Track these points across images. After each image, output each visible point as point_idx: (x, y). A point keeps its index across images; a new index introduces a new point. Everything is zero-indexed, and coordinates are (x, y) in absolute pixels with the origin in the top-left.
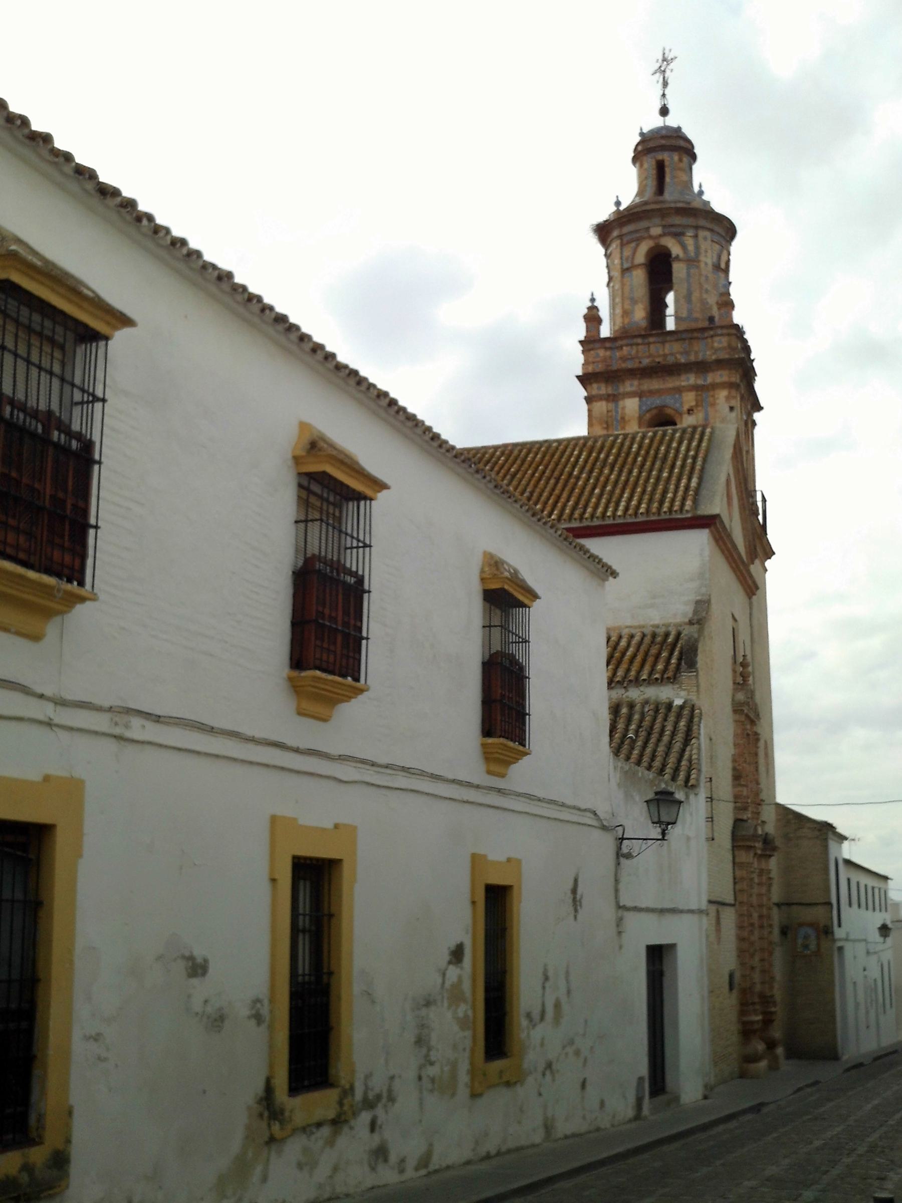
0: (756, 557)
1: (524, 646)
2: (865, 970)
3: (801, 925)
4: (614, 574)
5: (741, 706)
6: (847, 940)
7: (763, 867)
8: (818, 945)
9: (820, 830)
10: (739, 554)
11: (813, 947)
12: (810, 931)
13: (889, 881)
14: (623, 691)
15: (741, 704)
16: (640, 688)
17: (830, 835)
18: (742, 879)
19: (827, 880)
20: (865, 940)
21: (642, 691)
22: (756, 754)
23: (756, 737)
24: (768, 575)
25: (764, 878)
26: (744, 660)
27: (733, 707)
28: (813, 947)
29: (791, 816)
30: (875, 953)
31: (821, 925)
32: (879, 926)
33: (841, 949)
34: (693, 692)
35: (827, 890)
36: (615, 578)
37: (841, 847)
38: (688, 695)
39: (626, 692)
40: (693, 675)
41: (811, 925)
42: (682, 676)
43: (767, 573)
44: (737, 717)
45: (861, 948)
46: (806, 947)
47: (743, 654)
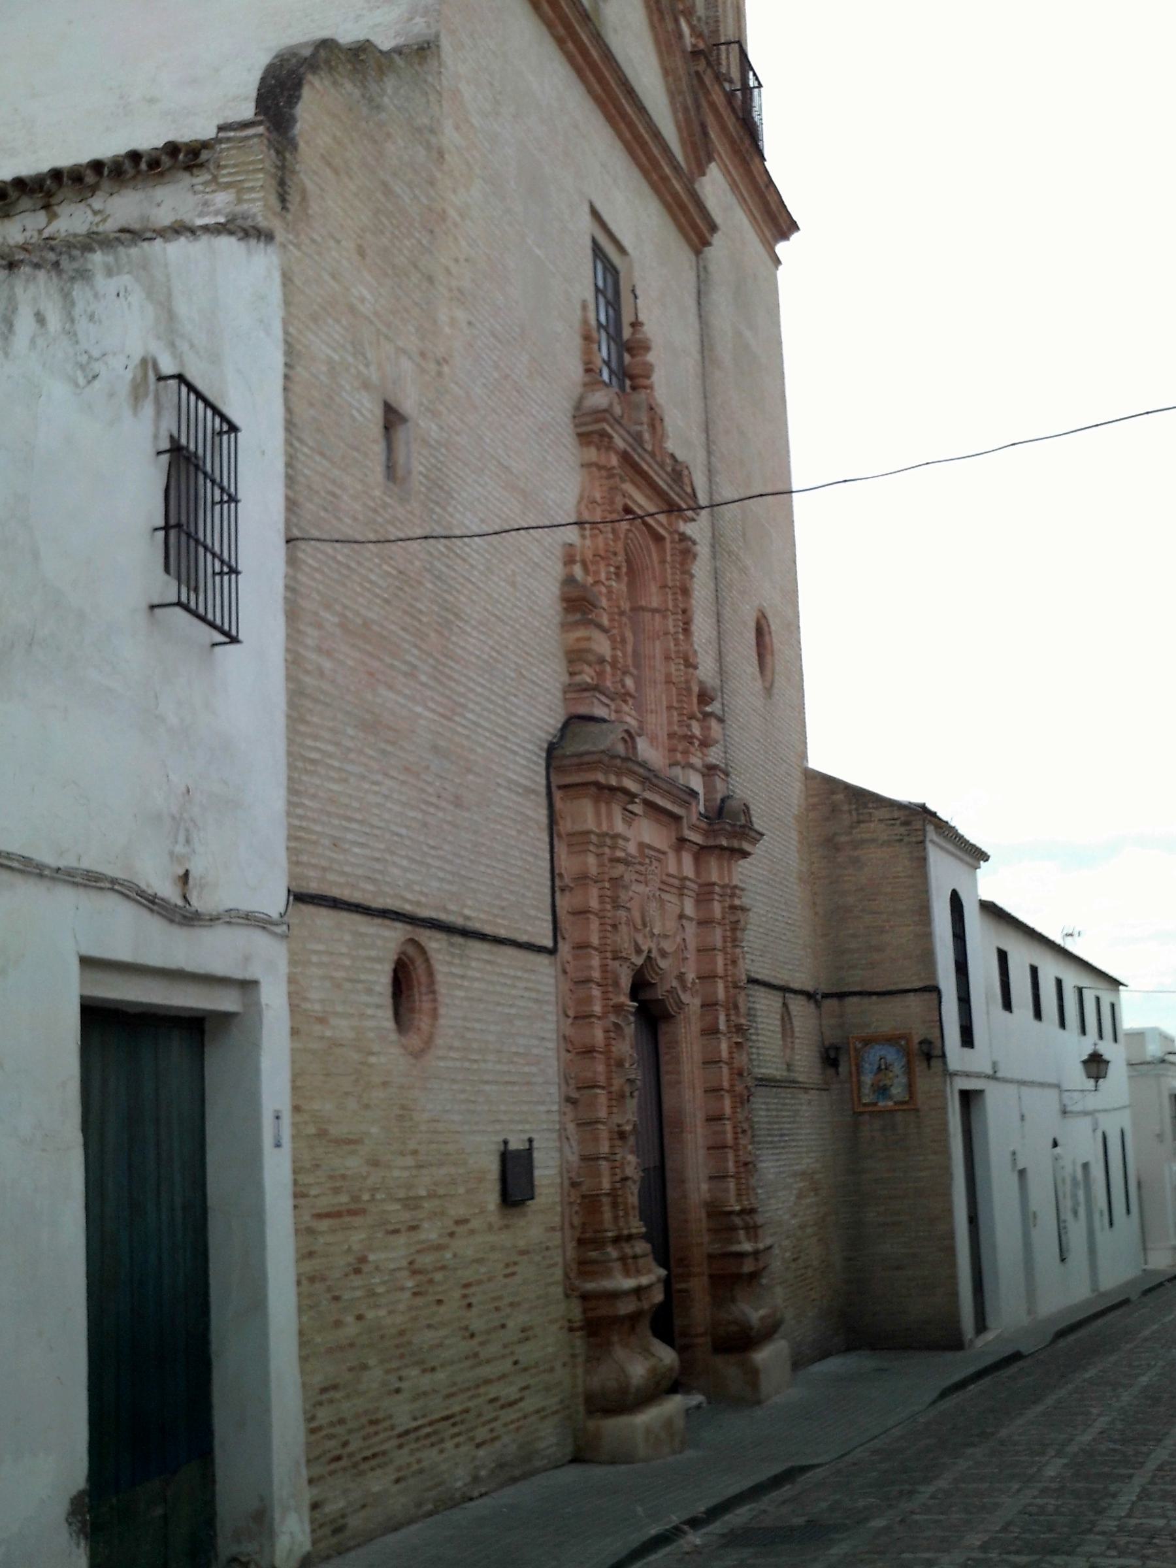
0: (710, 159)
1: (232, 439)
2: (1055, 1144)
3: (868, 1042)
4: (984, 857)
5: (597, 421)
6: (993, 1077)
7: (714, 878)
8: (910, 1087)
9: (906, 823)
10: (657, 135)
11: (898, 1091)
12: (890, 1054)
13: (1121, 988)
14: (41, 217)
15: (600, 415)
16: (90, 201)
17: (930, 830)
18: (583, 878)
19: (926, 936)
20: (1058, 1086)
21: (95, 213)
22: (685, 591)
23: (683, 545)
24: (782, 273)
25: (717, 909)
26: (633, 334)
27: (576, 426)
28: (898, 1091)
29: (840, 797)
30: (1086, 1113)
31: (916, 1040)
32: (1085, 1057)
33: (968, 1098)
34: (252, 189)
35: (928, 957)
36: (987, 860)
37: (975, 872)
38: (240, 201)
39: (49, 223)
40: (255, 136)
41: (891, 1040)
42: (222, 151)
43: (780, 268)
44: (592, 454)
45: (1043, 1104)
46: (882, 1090)
47: (633, 319)
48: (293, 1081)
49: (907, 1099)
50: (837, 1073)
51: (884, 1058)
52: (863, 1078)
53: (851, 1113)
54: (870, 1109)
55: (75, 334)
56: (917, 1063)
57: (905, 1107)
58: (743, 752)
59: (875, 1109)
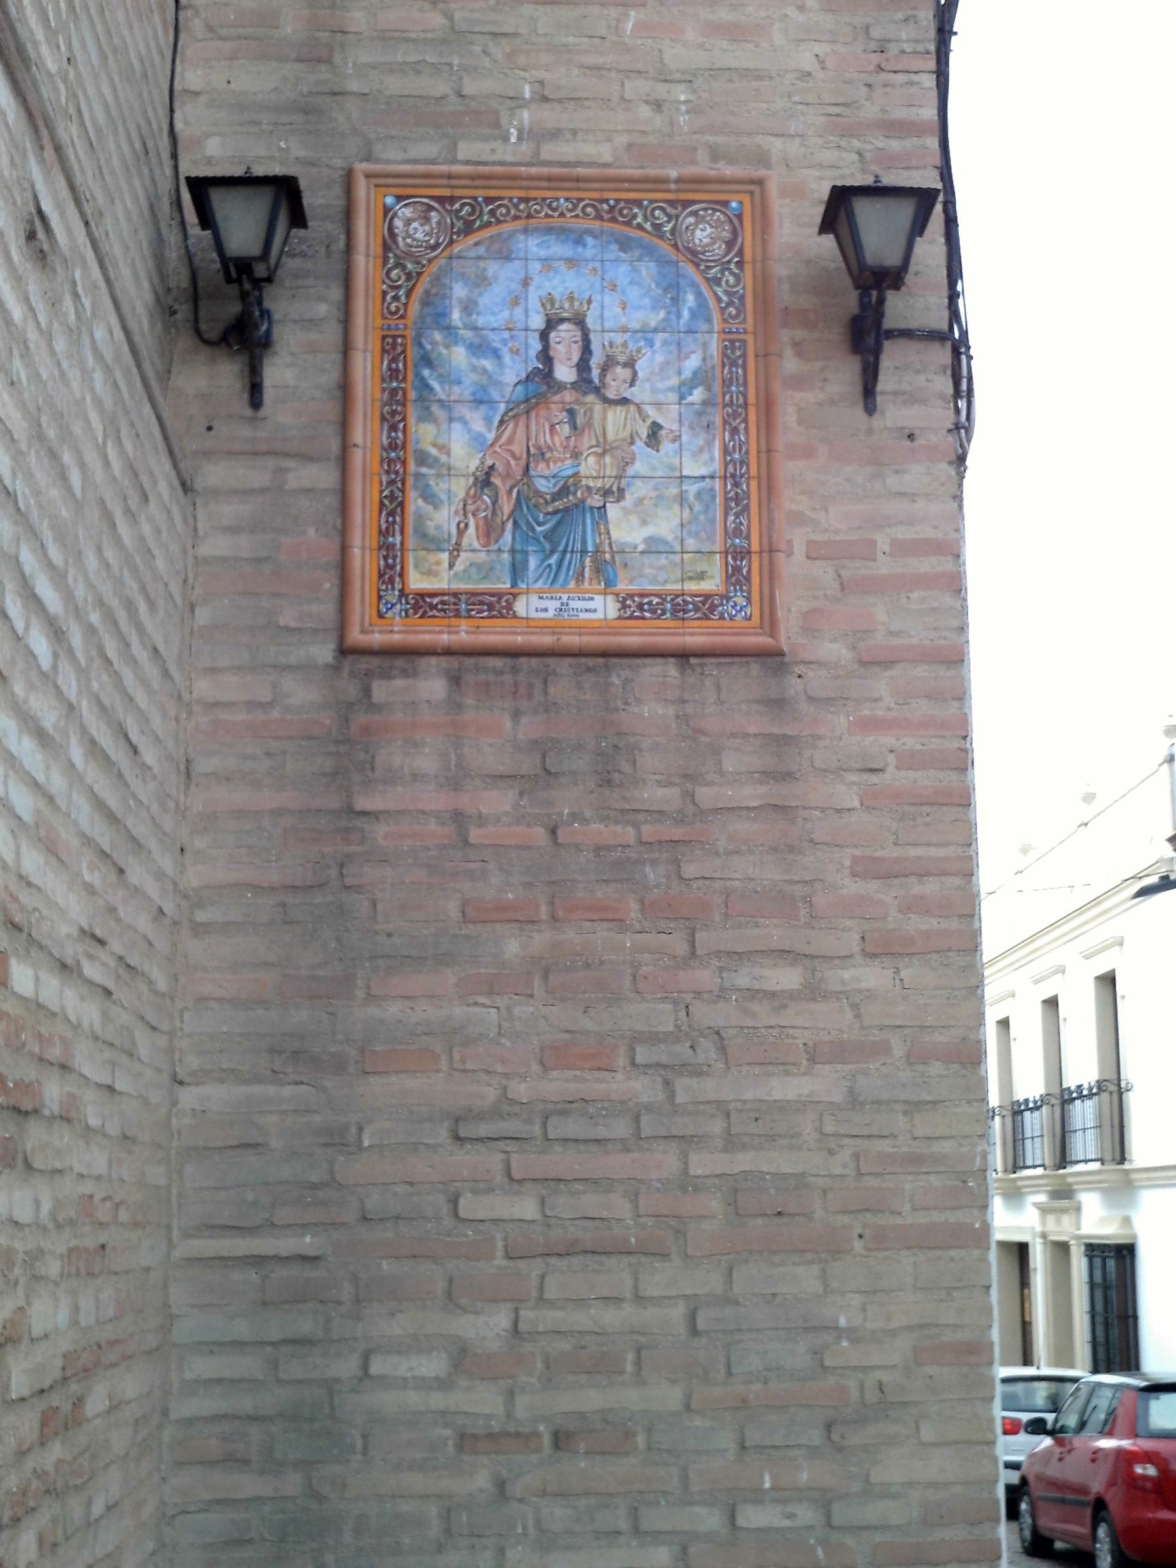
48: (961, 507)
49: (713, 584)
50: (255, 392)
51: (580, 322)
52: (423, 434)
53: (324, 652)
54: (463, 634)
55: (684, 1234)
56: (790, 364)
57: (695, 636)
58: (117, 98)
59: (495, 634)
